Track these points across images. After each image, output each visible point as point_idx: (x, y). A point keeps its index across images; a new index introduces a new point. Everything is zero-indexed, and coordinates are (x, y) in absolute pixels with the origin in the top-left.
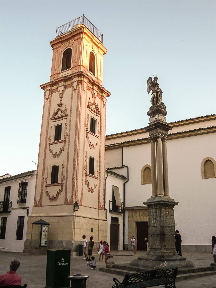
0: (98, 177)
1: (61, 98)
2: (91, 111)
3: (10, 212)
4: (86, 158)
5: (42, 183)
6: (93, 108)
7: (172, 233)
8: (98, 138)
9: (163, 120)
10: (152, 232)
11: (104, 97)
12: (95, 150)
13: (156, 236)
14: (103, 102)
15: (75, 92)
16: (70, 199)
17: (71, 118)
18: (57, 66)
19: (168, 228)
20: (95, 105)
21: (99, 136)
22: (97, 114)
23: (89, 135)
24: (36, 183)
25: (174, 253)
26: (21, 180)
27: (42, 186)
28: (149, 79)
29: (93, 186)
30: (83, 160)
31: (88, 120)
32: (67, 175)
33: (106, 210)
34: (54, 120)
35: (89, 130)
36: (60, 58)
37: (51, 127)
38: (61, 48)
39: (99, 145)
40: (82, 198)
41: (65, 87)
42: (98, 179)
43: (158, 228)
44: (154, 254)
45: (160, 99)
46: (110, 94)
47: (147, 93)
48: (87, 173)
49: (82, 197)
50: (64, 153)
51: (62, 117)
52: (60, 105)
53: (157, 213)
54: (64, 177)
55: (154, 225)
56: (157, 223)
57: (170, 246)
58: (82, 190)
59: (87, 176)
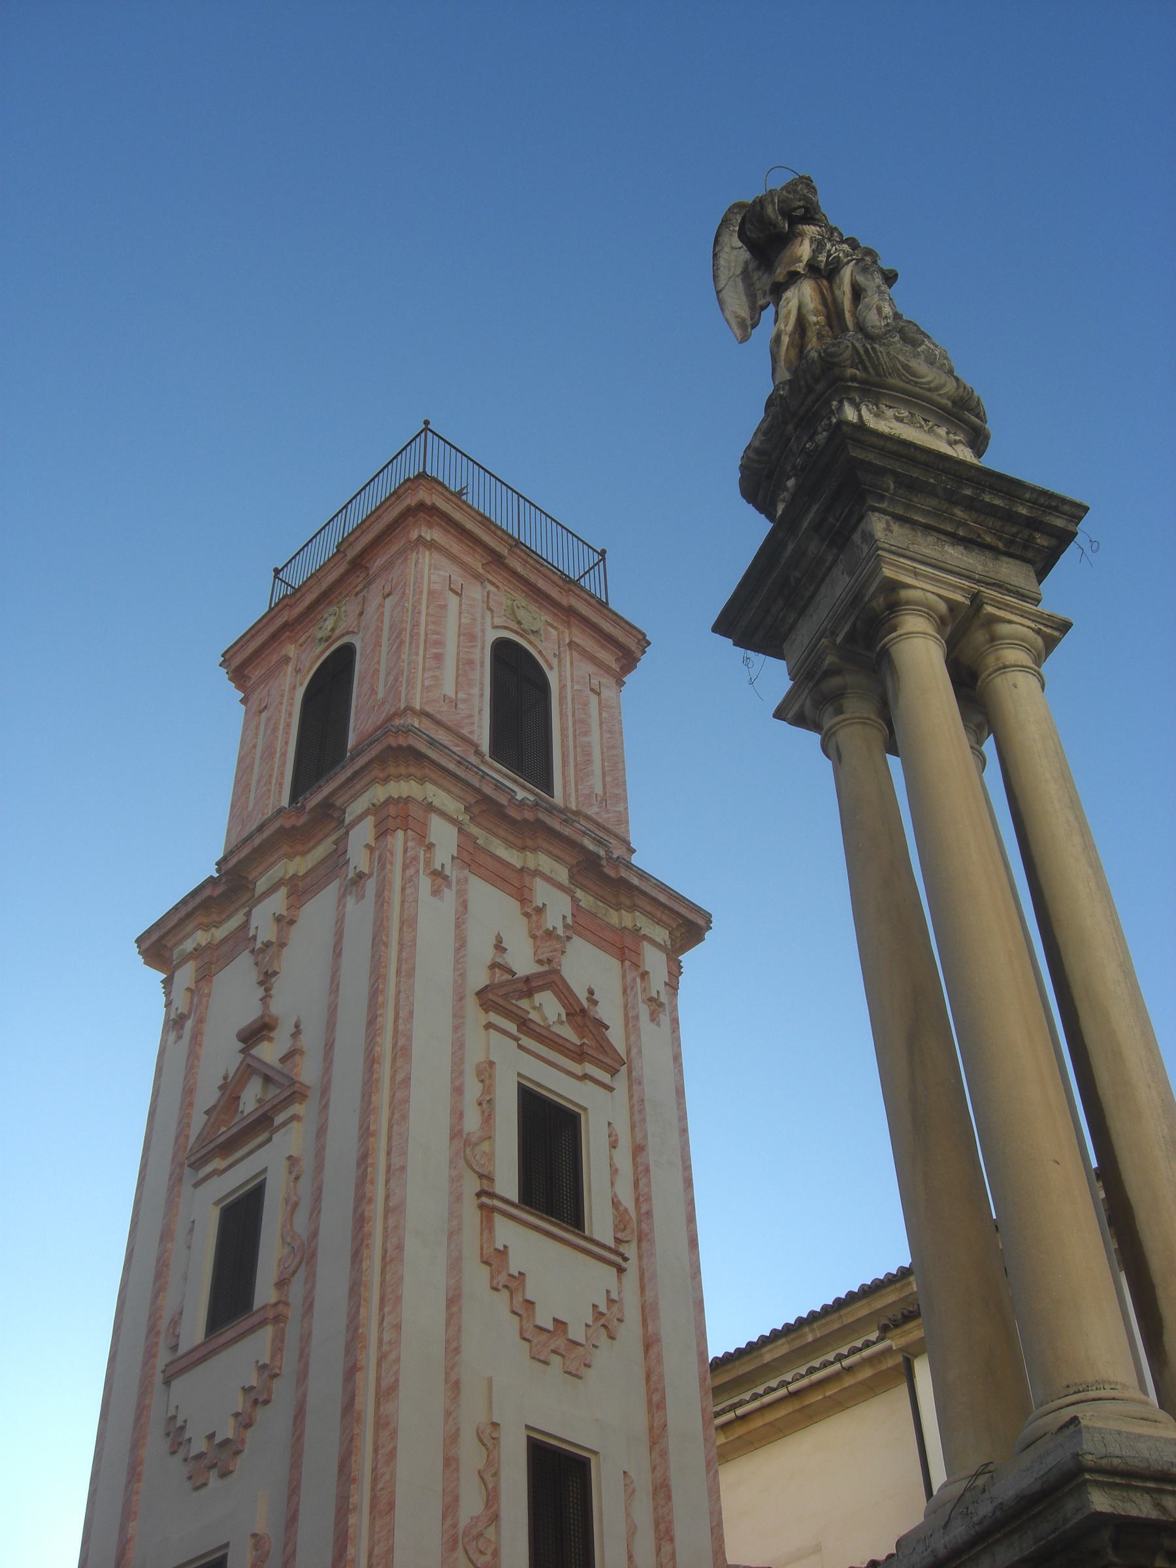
8: (621, 1270)
11: (645, 937)
18: (263, 783)
23: (506, 1232)
31: (487, 1105)
35: (508, 1183)
36: (281, 728)
38: (290, 668)
39: (631, 1332)
46: (701, 922)
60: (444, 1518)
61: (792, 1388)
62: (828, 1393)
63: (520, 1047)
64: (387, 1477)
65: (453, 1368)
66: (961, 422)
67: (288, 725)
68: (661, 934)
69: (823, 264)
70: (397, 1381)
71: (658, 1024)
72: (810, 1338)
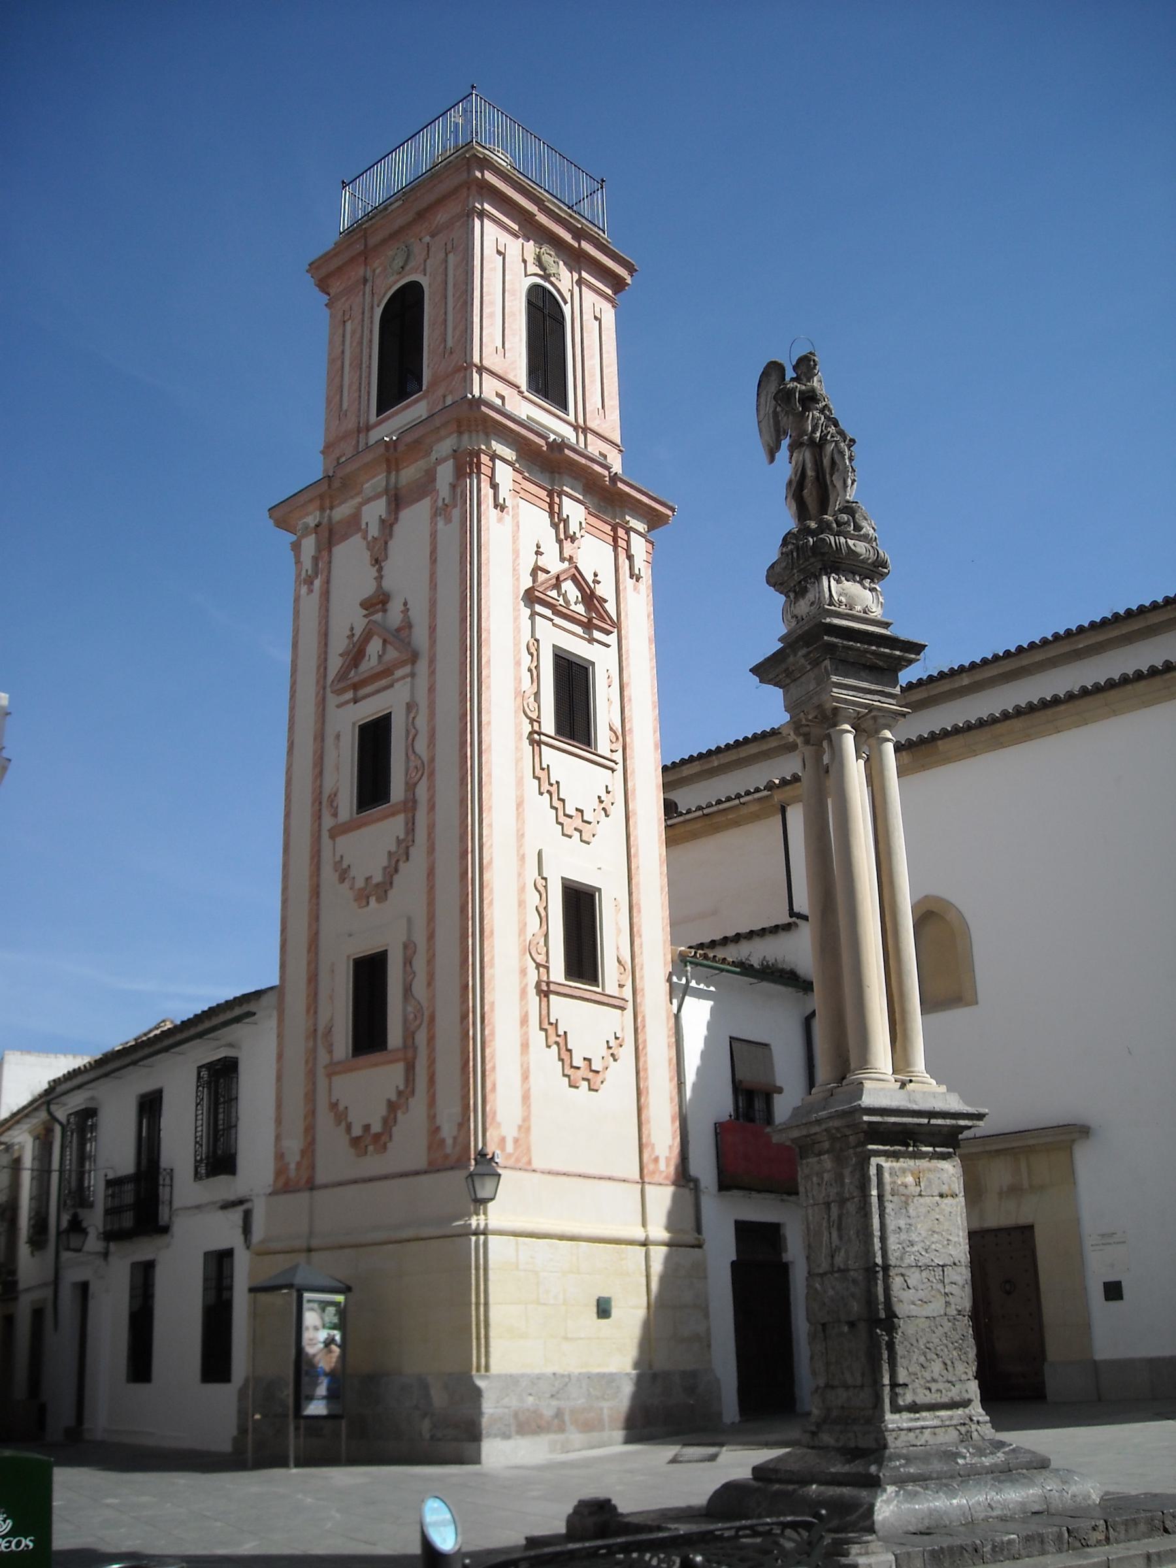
0: (627, 993)
1: (377, 562)
2: (551, 620)
3: (165, 1230)
4: (542, 891)
5: (312, 1054)
6: (567, 602)
7: (948, 1304)
8: (613, 770)
9: (858, 608)
10: (824, 1304)
12: (593, 840)
13: (846, 1329)
14: (630, 557)
15: (448, 520)
16: (455, 1138)
17: (432, 673)
19: (914, 1278)
20: (578, 579)
21: (618, 756)
22: (597, 634)
24: (280, 1056)
25: (963, 1429)
26: (206, 1052)
27: (311, 1074)
28: (765, 374)
29: (598, 1054)
30: (521, 904)
32: (432, 999)
33: (696, 1181)
34: (349, 695)
35: (548, 725)
37: (338, 737)
39: (618, 811)
40: (525, 1127)
41: (397, 501)
42: (630, 1005)
43: (854, 1282)
44: (837, 1440)
45: (839, 485)
47: (762, 455)
48: (552, 979)
49: (526, 1119)
50: (412, 874)
51: (387, 672)
52: (378, 602)
53: (842, 1184)
54: (420, 1009)
55: (832, 1265)
56: (847, 1252)
57: (934, 1386)
58: (525, 1077)
59: (552, 997)
60: (520, 936)
61: (705, 811)
62: (730, 817)
63: (554, 625)
64: (489, 916)
65: (521, 846)
66: (880, 691)
67: (371, 341)
68: (641, 526)
69: (818, 439)
70: (491, 858)
71: (638, 593)
72: (716, 764)
